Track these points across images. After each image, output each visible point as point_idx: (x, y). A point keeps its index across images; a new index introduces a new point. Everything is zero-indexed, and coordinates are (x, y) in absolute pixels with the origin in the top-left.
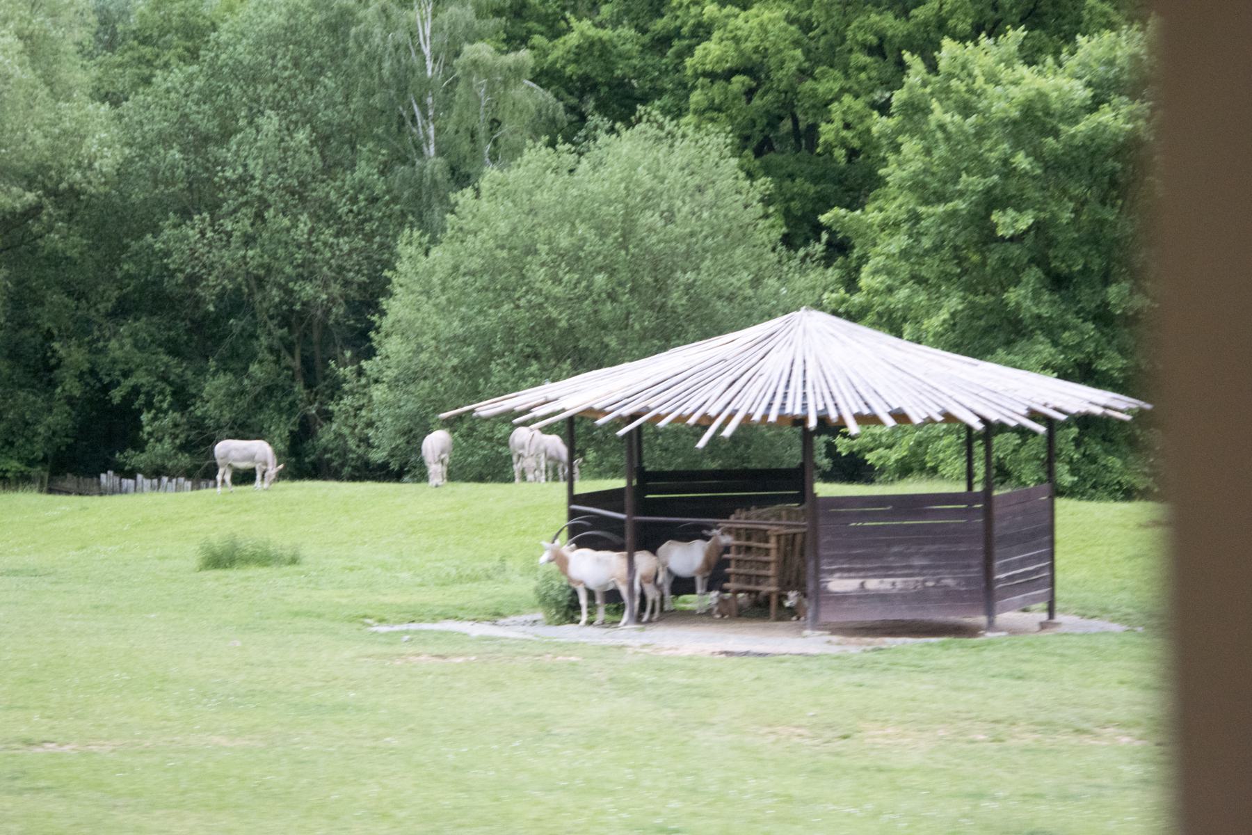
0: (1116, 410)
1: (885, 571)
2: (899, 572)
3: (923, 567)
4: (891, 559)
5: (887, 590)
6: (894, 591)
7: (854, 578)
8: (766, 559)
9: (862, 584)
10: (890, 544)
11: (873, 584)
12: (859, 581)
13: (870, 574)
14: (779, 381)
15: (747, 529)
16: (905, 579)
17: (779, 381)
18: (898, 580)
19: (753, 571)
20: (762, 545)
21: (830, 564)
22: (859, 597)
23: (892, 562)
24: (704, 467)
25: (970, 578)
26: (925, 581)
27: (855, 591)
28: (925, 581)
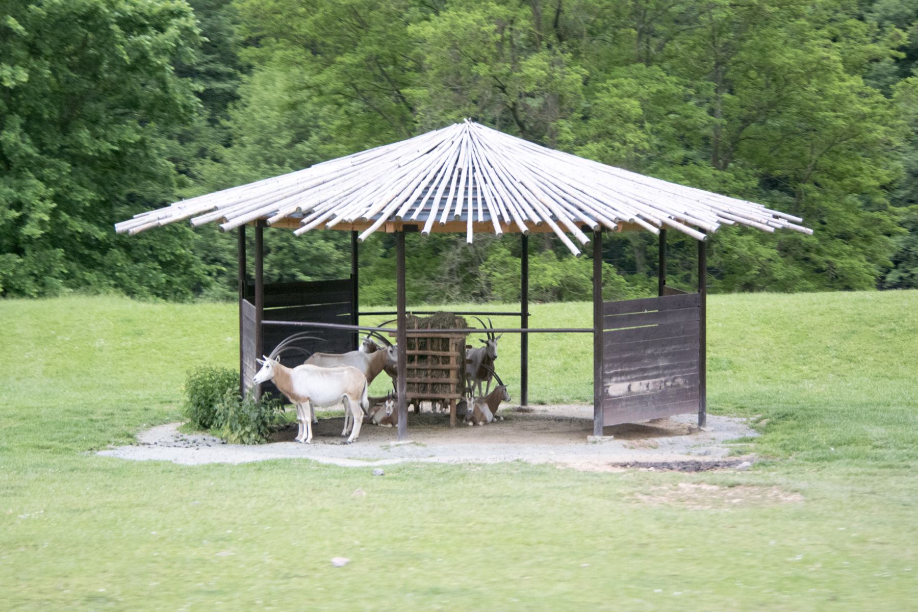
0: (755, 221)
1: (642, 374)
2: (650, 374)
3: (666, 368)
4: (646, 361)
5: (643, 392)
6: (648, 392)
7: (622, 381)
8: (446, 366)
9: (629, 387)
10: (646, 346)
11: (637, 387)
12: (626, 385)
13: (634, 377)
14: (320, 216)
15: (419, 338)
16: (654, 380)
17: (320, 216)
18: (650, 381)
19: (430, 380)
20: (441, 353)
21: (610, 368)
22: (627, 400)
23: (647, 364)
24: (520, 274)
25: (692, 376)
26: (665, 382)
27: (624, 395)
28: (665, 382)
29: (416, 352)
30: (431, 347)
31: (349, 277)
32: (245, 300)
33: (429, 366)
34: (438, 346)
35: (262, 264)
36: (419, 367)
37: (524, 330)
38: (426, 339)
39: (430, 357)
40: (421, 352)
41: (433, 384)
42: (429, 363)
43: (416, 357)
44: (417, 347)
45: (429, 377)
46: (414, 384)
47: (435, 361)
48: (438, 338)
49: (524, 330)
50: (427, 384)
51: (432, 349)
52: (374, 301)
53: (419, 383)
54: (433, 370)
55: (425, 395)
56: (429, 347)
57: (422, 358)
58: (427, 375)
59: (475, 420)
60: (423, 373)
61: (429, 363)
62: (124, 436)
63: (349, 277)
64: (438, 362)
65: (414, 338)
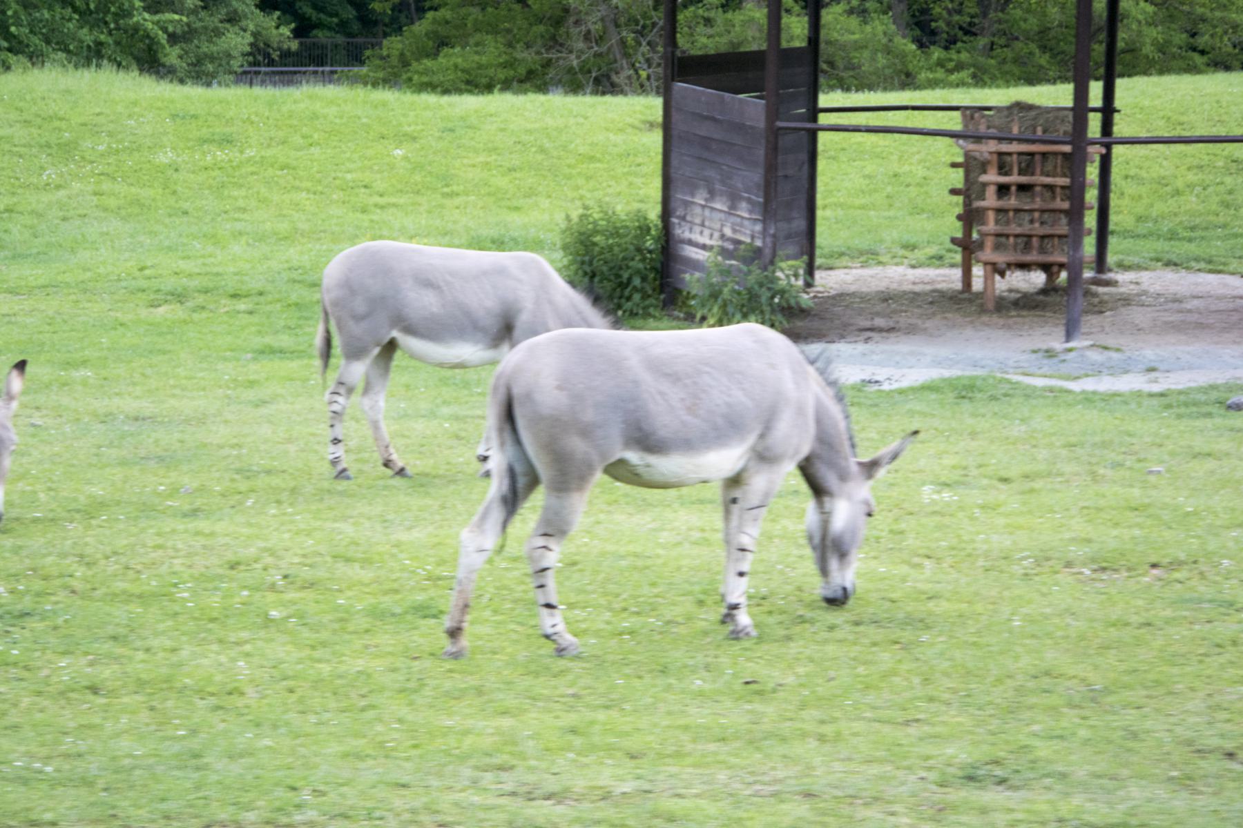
15: (1020, 154)
19: (1038, 229)
29: (1014, 178)
30: (1042, 170)
31: (804, 44)
32: (680, 85)
33: (1038, 203)
34: (1055, 167)
35: (779, 18)
36: (1020, 207)
37: (1106, 140)
38: (1032, 154)
39: (1038, 189)
40: (1024, 179)
41: (1043, 237)
42: (1038, 199)
43: (1013, 189)
44: (1016, 170)
45: (1037, 225)
46: (1007, 236)
47: (1048, 194)
48: (1055, 154)
49: (1106, 140)
50: (1030, 236)
51: (1043, 174)
52: (447, 85)
53: (1017, 236)
54: (1043, 211)
55: (1028, 258)
56: (1038, 171)
57: (1023, 188)
58: (1032, 221)
59: (636, 314)
60: (1027, 217)
61: (1038, 199)
62: (815, 315)
63: (804, 44)
64: (1054, 198)
65: (1010, 154)
